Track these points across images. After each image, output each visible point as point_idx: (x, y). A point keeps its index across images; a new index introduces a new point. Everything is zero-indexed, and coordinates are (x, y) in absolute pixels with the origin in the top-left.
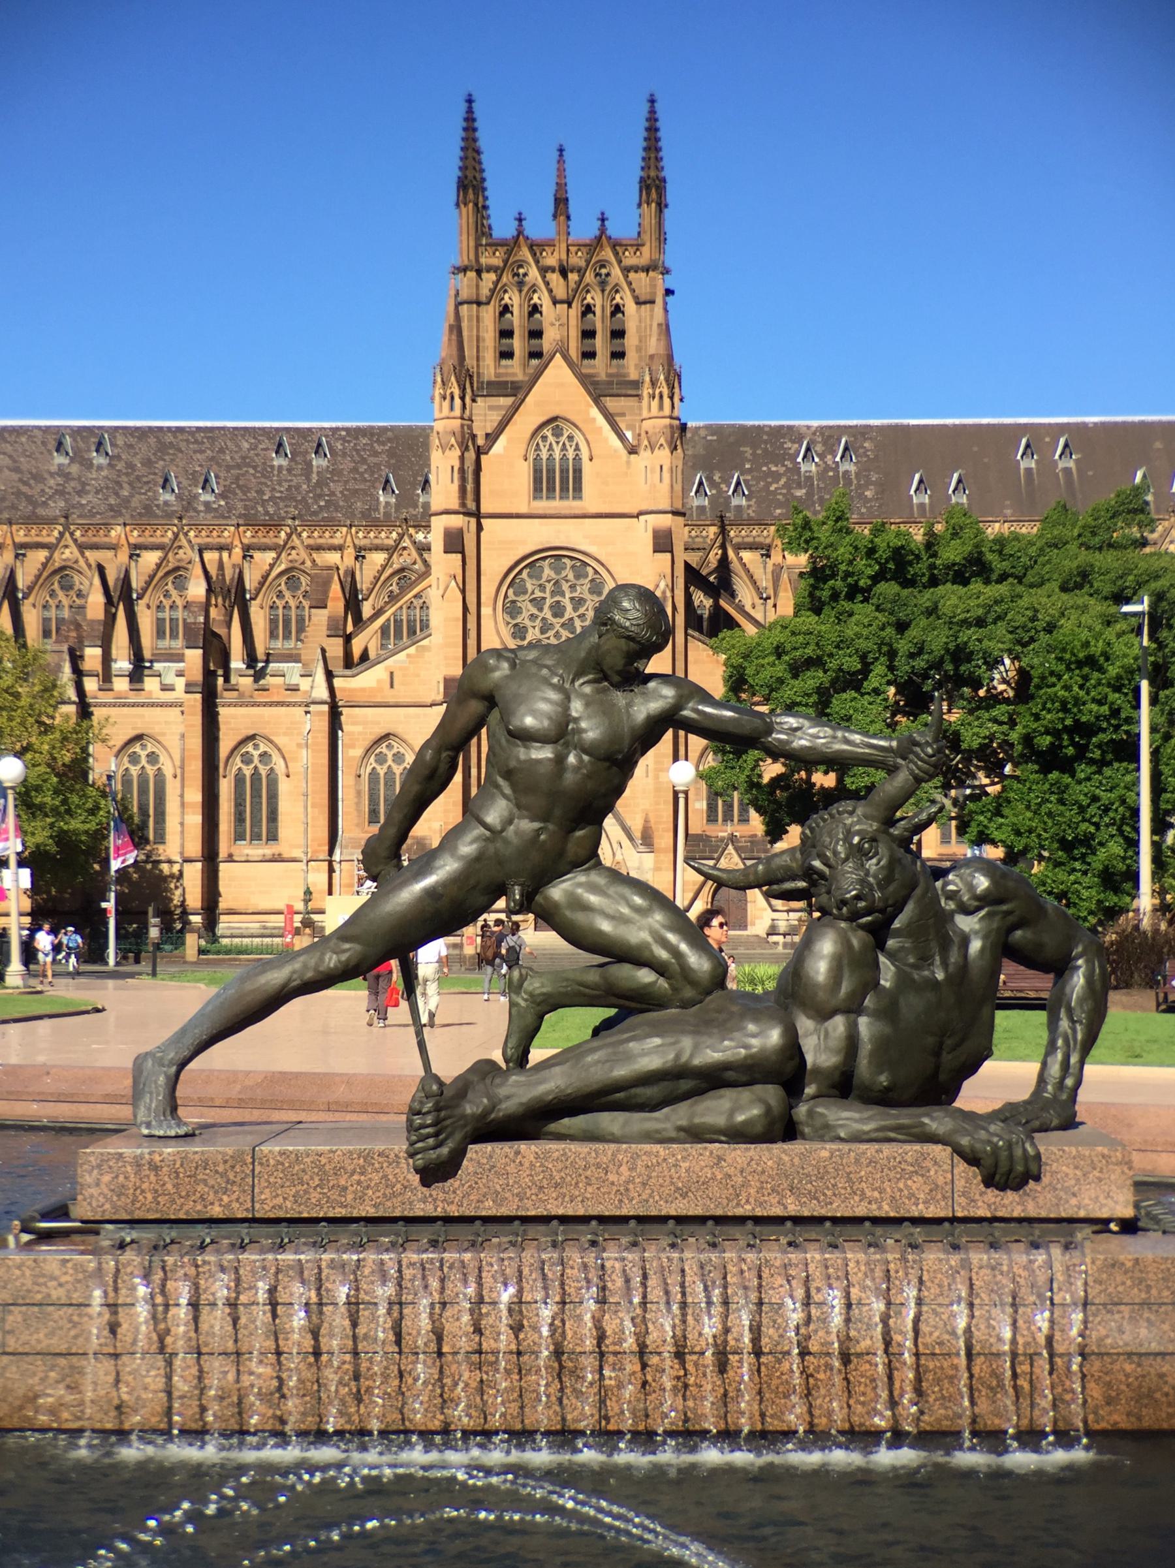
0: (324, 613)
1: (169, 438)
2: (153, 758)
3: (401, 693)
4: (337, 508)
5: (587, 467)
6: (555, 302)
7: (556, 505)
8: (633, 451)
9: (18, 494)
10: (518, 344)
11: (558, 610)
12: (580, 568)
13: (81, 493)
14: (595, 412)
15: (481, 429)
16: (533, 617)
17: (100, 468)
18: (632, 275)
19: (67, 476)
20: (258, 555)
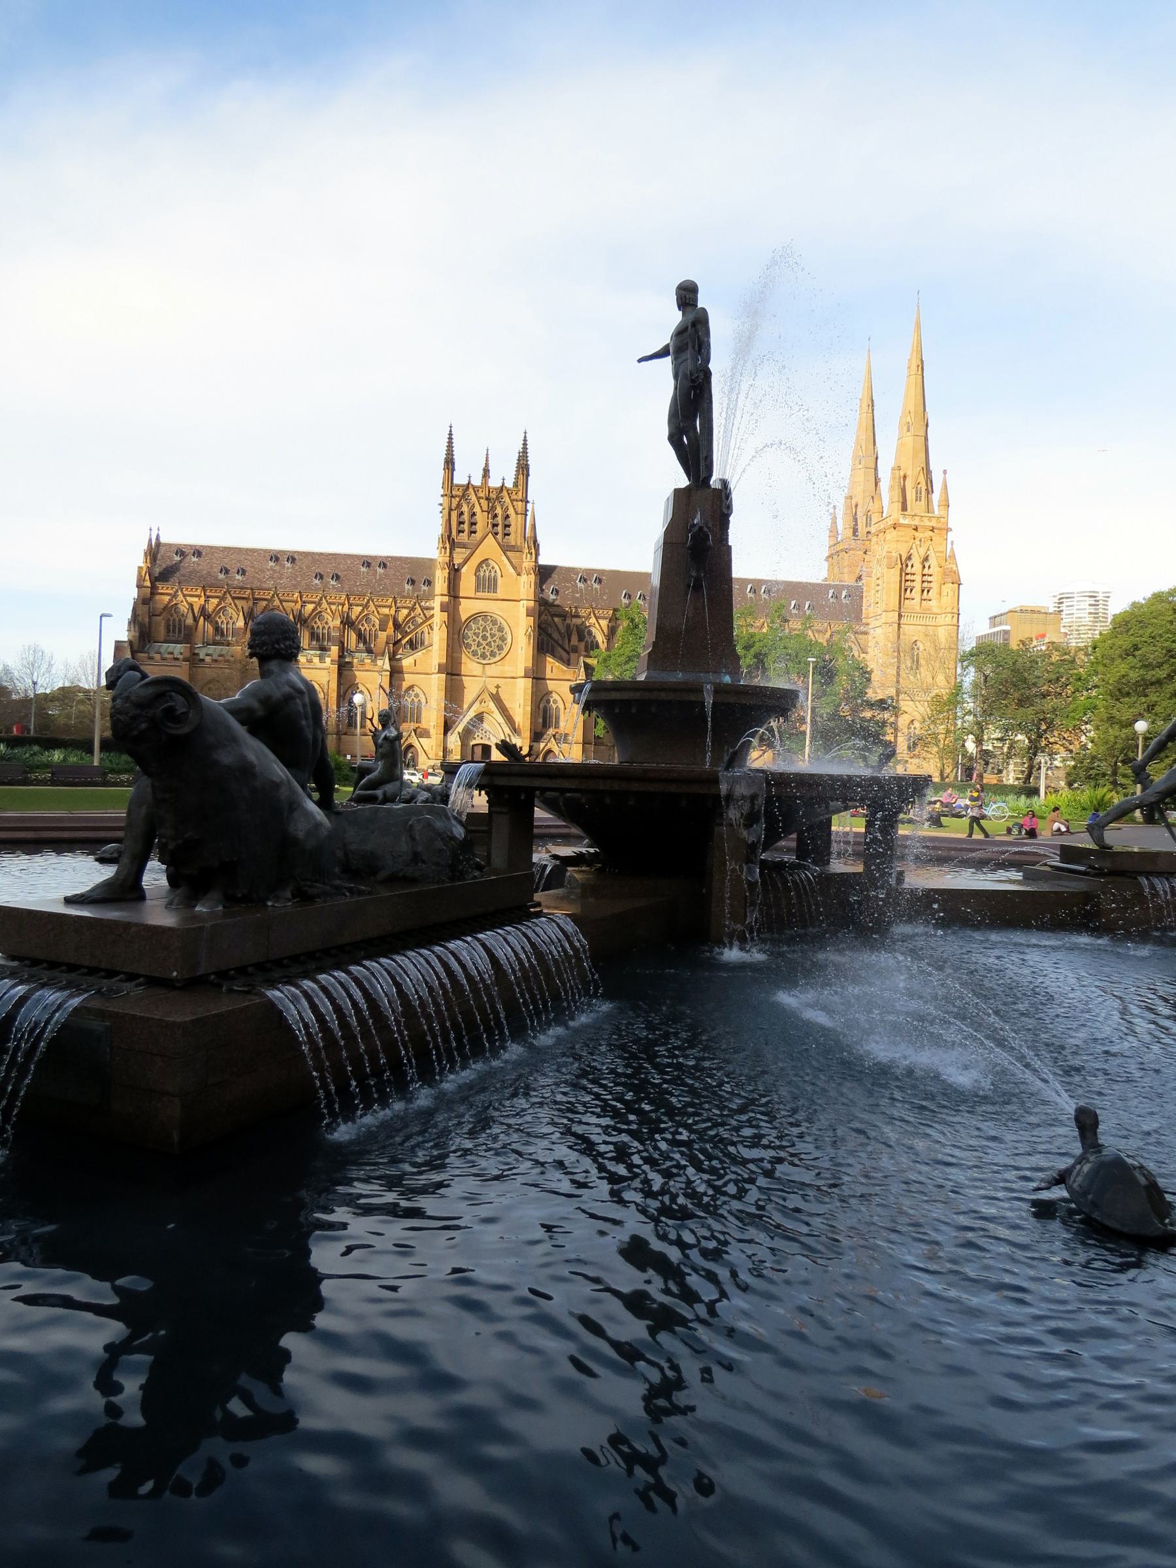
0: (385, 634)
1: (317, 557)
2: (417, 695)
3: (419, 669)
4: (388, 590)
5: (500, 580)
6: (517, 513)
7: (486, 595)
8: (519, 575)
9: (254, 577)
10: (466, 527)
11: (485, 638)
12: (494, 622)
13: (280, 578)
14: (504, 558)
15: (458, 561)
16: (494, 641)
17: (288, 568)
18: (515, 503)
19: (274, 571)
20: (212, 600)
